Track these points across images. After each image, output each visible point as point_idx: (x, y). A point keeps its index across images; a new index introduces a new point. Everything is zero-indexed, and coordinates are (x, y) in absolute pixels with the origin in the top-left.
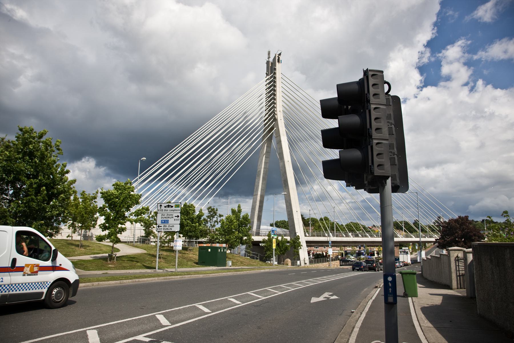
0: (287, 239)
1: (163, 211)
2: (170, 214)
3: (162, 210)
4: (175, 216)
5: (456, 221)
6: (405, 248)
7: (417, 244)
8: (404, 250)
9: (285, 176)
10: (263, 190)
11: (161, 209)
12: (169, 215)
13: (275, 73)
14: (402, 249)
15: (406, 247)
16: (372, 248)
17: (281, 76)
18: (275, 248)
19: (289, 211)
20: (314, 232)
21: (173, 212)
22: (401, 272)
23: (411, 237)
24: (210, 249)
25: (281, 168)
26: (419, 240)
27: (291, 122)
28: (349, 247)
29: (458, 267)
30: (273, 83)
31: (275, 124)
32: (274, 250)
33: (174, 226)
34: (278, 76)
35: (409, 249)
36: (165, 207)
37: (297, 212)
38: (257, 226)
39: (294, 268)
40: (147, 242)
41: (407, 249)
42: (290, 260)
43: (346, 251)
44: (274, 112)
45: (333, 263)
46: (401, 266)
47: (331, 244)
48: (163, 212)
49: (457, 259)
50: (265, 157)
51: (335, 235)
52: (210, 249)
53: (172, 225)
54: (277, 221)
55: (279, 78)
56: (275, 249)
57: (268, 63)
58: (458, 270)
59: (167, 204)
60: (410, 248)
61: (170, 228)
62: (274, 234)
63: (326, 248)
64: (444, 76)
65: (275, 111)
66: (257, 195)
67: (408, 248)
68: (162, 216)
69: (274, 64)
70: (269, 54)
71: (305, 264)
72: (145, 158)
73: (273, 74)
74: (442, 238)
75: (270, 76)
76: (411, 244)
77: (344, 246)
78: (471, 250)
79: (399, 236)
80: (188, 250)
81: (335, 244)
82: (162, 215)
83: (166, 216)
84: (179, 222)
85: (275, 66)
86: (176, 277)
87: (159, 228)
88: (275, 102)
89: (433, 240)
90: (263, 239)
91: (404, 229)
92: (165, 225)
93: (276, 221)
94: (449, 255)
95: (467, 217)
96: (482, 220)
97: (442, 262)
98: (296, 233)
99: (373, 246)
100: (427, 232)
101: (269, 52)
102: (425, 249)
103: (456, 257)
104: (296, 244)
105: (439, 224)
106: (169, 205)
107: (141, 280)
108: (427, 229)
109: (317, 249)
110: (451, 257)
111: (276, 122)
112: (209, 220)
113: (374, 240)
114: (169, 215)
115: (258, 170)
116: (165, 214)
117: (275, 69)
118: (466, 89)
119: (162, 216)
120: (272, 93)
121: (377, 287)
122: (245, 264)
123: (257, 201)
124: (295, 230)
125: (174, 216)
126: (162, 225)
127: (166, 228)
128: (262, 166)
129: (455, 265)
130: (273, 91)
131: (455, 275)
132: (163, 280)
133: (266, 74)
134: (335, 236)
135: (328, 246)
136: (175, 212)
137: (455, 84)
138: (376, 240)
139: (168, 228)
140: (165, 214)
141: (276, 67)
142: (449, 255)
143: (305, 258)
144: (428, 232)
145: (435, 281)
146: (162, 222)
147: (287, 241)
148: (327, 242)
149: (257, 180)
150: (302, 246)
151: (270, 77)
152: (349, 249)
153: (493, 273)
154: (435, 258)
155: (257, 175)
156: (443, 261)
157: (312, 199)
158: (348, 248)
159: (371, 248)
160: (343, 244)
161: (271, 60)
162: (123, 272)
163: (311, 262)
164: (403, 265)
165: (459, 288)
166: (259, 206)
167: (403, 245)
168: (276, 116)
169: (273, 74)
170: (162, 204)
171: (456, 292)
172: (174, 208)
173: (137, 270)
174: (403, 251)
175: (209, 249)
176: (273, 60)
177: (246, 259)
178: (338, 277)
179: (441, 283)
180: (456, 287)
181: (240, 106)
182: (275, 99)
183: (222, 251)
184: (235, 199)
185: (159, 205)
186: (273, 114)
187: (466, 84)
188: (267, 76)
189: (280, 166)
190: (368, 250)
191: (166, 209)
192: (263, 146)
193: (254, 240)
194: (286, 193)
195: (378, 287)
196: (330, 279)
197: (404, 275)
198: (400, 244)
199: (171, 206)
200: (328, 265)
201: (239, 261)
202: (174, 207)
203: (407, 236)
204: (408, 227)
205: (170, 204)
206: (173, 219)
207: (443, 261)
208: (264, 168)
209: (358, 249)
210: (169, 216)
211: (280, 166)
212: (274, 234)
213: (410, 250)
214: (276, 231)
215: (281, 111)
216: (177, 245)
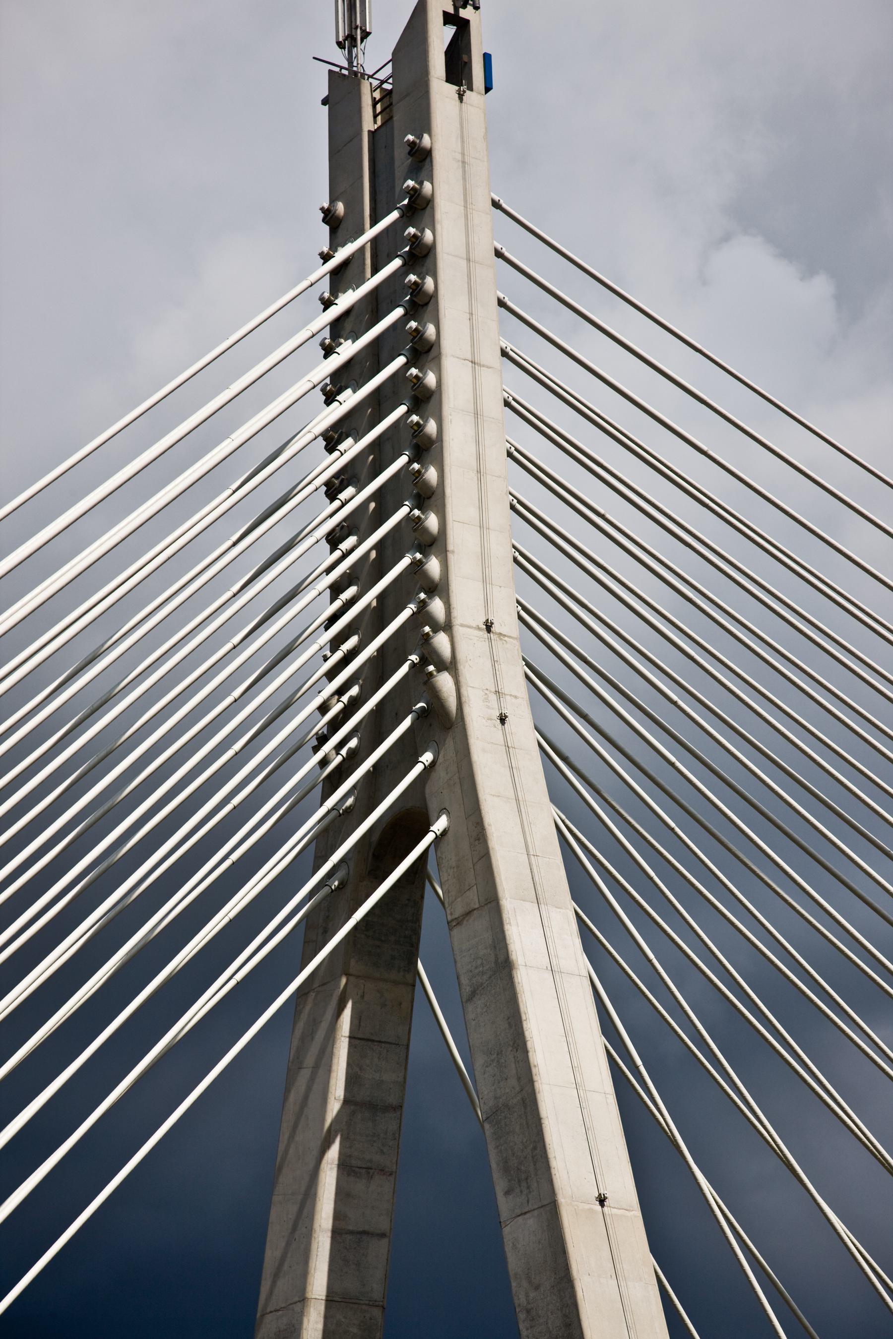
24: (422, 593)
25: (520, 1294)
31: (440, 772)
50: (344, 1166)
65: (436, 628)
75: (371, 233)
85: (424, 124)
88: (432, 522)
111: (450, 744)
130: (402, 409)
133: (329, 216)
141: (426, 140)
151: (375, 241)
168: (444, 682)
169: (395, 215)
188: (336, 242)
189: (514, 1263)
208: (330, 1300)
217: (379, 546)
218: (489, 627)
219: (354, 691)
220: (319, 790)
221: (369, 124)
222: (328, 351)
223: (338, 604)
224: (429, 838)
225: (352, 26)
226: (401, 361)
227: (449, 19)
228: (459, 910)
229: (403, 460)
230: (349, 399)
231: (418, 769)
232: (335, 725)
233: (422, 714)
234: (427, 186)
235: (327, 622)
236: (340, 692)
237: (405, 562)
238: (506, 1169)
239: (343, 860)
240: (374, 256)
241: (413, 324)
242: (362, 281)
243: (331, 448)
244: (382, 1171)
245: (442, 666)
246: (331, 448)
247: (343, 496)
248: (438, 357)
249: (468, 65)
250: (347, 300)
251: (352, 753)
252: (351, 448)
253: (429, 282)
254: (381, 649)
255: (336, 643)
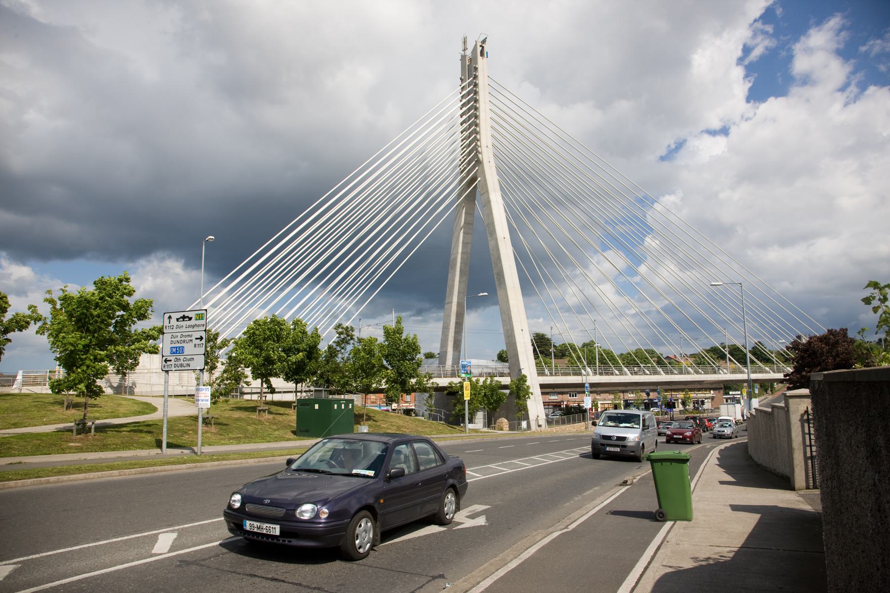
3: (172, 327)
4: (196, 339)
5: (823, 339)
6: (734, 393)
7: (758, 385)
8: (732, 396)
11: (170, 325)
12: (186, 336)
13: (476, 77)
14: (729, 394)
17: (487, 81)
20: (569, 366)
21: (193, 330)
23: (767, 372)
24: (317, 405)
25: (491, 252)
26: (747, 379)
32: (467, 403)
35: (741, 394)
36: (178, 320)
37: (522, 330)
38: (453, 359)
39: (516, 435)
41: (738, 394)
42: (506, 421)
43: (626, 401)
44: (475, 148)
47: (589, 388)
49: (805, 417)
50: (464, 233)
52: (317, 405)
53: (190, 357)
54: (503, 350)
55: (484, 85)
56: (468, 400)
57: (463, 58)
58: (808, 443)
59: (181, 314)
60: (743, 392)
61: (188, 362)
66: (452, 302)
67: (739, 393)
68: (172, 339)
69: (473, 60)
70: (464, 42)
71: (540, 426)
72: (213, 238)
73: (472, 78)
74: (797, 370)
75: (468, 81)
76: (745, 384)
77: (623, 392)
78: (805, 391)
80: (293, 407)
81: (596, 388)
82: (173, 337)
83: (179, 339)
85: (476, 63)
86: (178, 466)
88: (478, 129)
89: (780, 376)
90: (450, 384)
91: (729, 358)
92: (177, 357)
93: (501, 350)
95: (844, 331)
96: (879, 340)
97: (776, 423)
98: (520, 370)
99: (675, 390)
100: (774, 363)
101: (465, 39)
102: (772, 393)
103: (803, 412)
104: (519, 391)
105: (795, 346)
107: (65, 478)
109: (575, 398)
110: (791, 413)
111: (481, 166)
112: (338, 349)
114: (186, 336)
115: (452, 257)
117: (476, 69)
119: (173, 339)
120: (472, 113)
123: (452, 313)
125: (193, 338)
126: (173, 358)
129: (801, 433)
130: (473, 111)
131: (802, 455)
132: (135, 474)
133: (461, 79)
134: (598, 373)
135: (584, 392)
139: (183, 362)
140: (177, 334)
142: (786, 409)
143: (538, 416)
144: (775, 362)
145: (764, 464)
146: (172, 353)
148: (582, 385)
149: (450, 276)
151: (469, 83)
152: (631, 396)
157: (568, 309)
158: (629, 396)
159: (671, 395)
160: (621, 388)
161: (469, 53)
163: (549, 422)
165: (811, 487)
166: (457, 323)
168: (480, 156)
169: (472, 78)
170: (172, 315)
172: (193, 322)
173: (120, 452)
174: (730, 398)
175: (316, 405)
177: (410, 422)
179: (774, 470)
180: (804, 484)
181: (438, 153)
183: (343, 408)
185: (167, 316)
186: (475, 152)
188: (462, 83)
189: (490, 247)
190: (665, 397)
191: (179, 323)
193: (440, 386)
197: (655, 464)
198: (724, 386)
199: (188, 317)
200: (584, 428)
202: (193, 319)
203: (734, 372)
204: (741, 354)
205: (186, 314)
206: (191, 345)
207: (778, 422)
209: (644, 395)
213: (744, 395)
215: (490, 146)
216: (200, 398)
217: (469, 133)
219: (465, 157)
220: (459, 174)
221: (468, 63)
223: (462, 143)
225: (465, 47)
228: (482, 193)
231: (475, 170)
232: (462, 163)
233: (476, 161)
235: (624, 416)
236: (463, 157)
237: (474, 136)
238: (489, 233)
239: (464, 185)
240: (469, 85)
241: (475, 89)
244: (470, 233)
249: (484, 53)
250: (464, 93)
251: (465, 167)
254: (470, 150)
255: (462, 149)
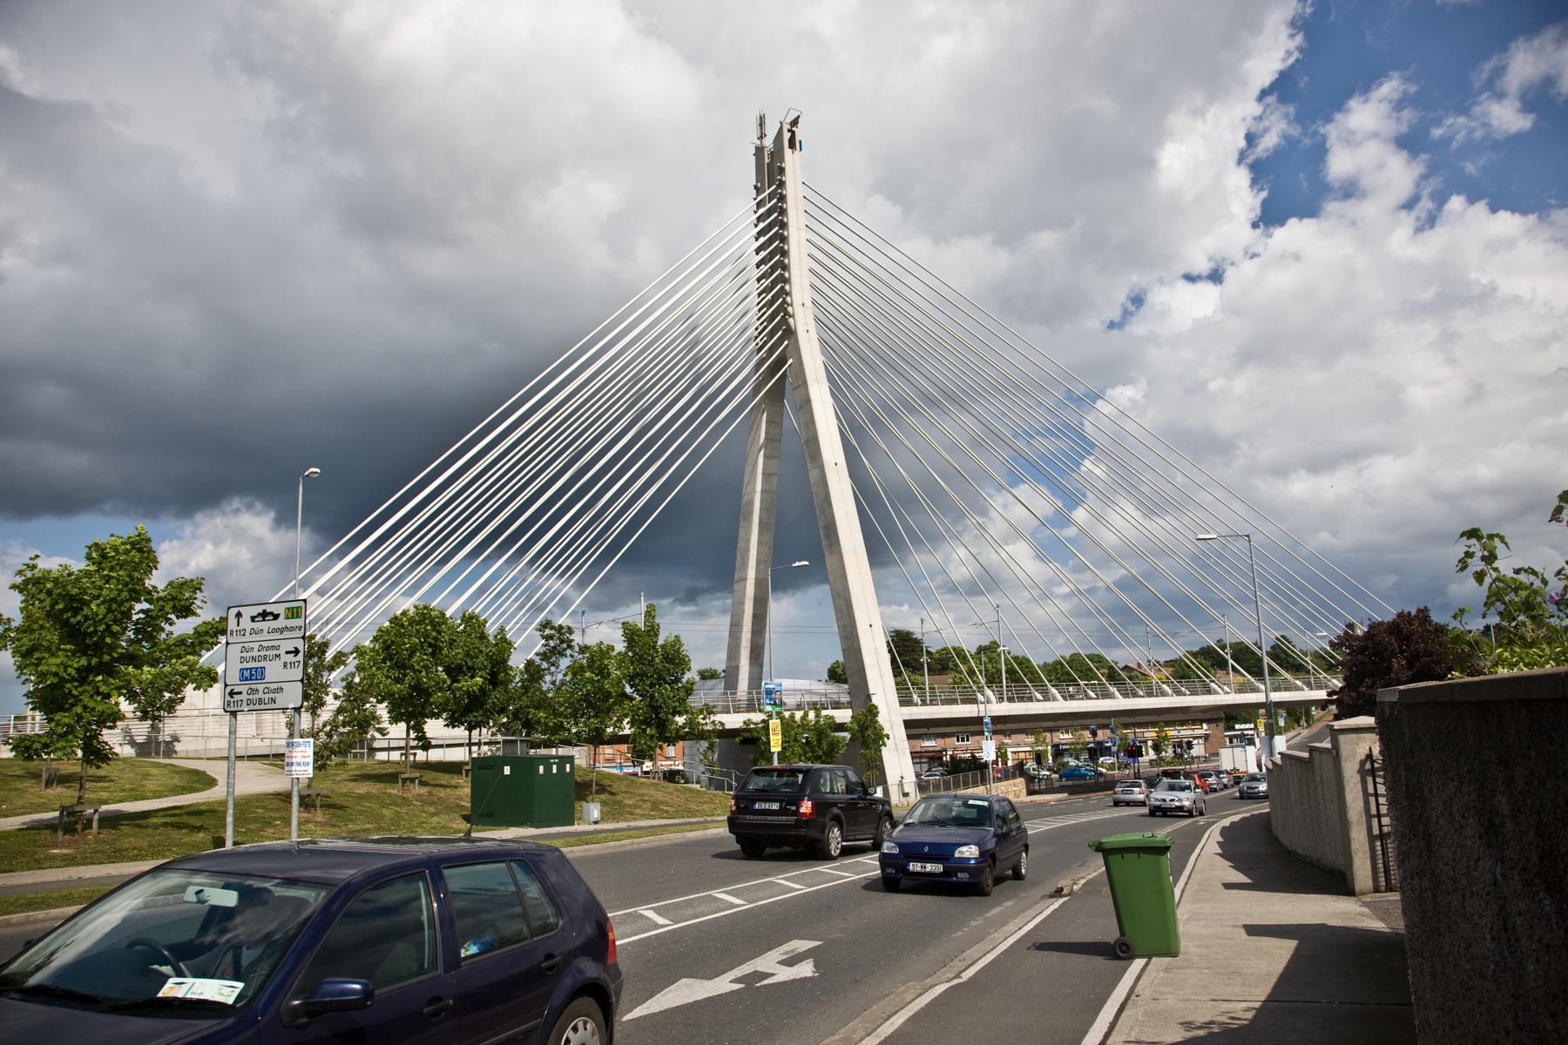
0: (832, 717)
1: (247, 633)
2: (270, 644)
3: (242, 633)
4: (287, 652)
6: (1243, 726)
7: (1283, 712)
8: (1239, 732)
9: (826, 512)
10: (765, 562)
11: (238, 628)
12: (268, 648)
13: (782, 184)
15: (1246, 723)
16: (1138, 730)
17: (803, 190)
18: (779, 749)
19: (845, 627)
21: (282, 637)
22: (1100, 843)
25: (814, 489)
27: (839, 333)
28: (1067, 733)
29: (1372, 799)
30: (776, 214)
31: (790, 348)
32: (776, 757)
33: (282, 689)
34: (793, 190)
35: (1256, 728)
36: (253, 619)
37: (871, 626)
38: (749, 679)
40: (358, 751)
41: (1251, 729)
43: (1056, 746)
44: (783, 308)
45: (1003, 788)
46: (1226, 787)
47: (990, 726)
48: (248, 638)
49: (1368, 766)
50: (765, 456)
51: (1005, 697)
56: (779, 753)
57: (759, 151)
58: (1374, 812)
61: (271, 695)
62: (772, 702)
63: (971, 742)
64: (1337, 185)
65: (788, 305)
67: (1252, 726)
68: (243, 655)
69: (777, 154)
70: (761, 124)
71: (906, 795)
72: (319, 471)
73: (774, 186)
75: (768, 192)
76: (1262, 711)
77: (1051, 730)
78: (1367, 721)
79: (1214, 690)
80: (464, 772)
81: (1004, 725)
82: (244, 650)
83: (256, 653)
84: (298, 673)
85: (782, 160)
87: (232, 700)
88: (787, 275)
91: (1233, 666)
92: (253, 687)
93: (834, 661)
94: (1334, 751)
96: (1485, 627)
97: (1318, 778)
98: (869, 697)
99: (1141, 725)
100: (1309, 670)
101: (761, 118)
103: (1363, 757)
105: (1345, 641)
106: (264, 611)
108: (1308, 664)
109: (966, 743)
110: (1343, 759)
112: (545, 665)
113: (1133, 705)
114: (268, 648)
115: (745, 499)
116: (251, 645)
117: (782, 171)
118: (1407, 222)
119: (244, 654)
121: (1062, 889)
122: (666, 812)
124: (867, 686)
125: (282, 651)
126: (244, 689)
127: (257, 696)
128: (755, 485)
129: (1361, 794)
130: (778, 242)
131: (1365, 832)
133: (756, 187)
134: (1005, 699)
135: (981, 733)
136: (286, 634)
137: (1368, 210)
138: (1140, 704)
139: (262, 696)
140: (251, 645)
141: (783, 165)
142: (1334, 751)
143: (902, 778)
144: (1312, 671)
145: (1300, 851)
146: (243, 678)
147: (835, 723)
148: (978, 721)
149: (742, 533)
150: (888, 738)
151: (769, 194)
152: (1064, 737)
153: (1505, 929)
154: (1294, 762)
155: (741, 517)
156: (1321, 776)
158: (1062, 737)
160: (1046, 724)
161: (769, 142)
162: (50, 879)
164: (1232, 783)
165: (1383, 889)
166: (755, 616)
167: (1239, 717)
168: (791, 321)
169: (774, 186)
171: (1366, 910)
172: (281, 623)
174: (1236, 736)
176: (774, 142)
178: (1045, 825)
180: (1369, 884)
182: (785, 267)
183: (555, 771)
184: (716, 603)
186: (782, 314)
187: (1409, 205)
188: (758, 195)
189: (812, 481)
191: (256, 625)
192: (758, 421)
193: (727, 727)
194: (807, 563)
195: (1065, 891)
196: (1052, 825)
198: (1226, 715)
199: (271, 613)
201: (646, 801)
205: (269, 609)
206: (279, 664)
207: (1321, 776)
208: (762, 492)
209: (1087, 735)
210: (267, 653)
211: (809, 481)
212: (772, 702)
213: (1260, 730)
214: (780, 691)
215: (808, 303)
216: (294, 760)
217: (771, 282)
218: (803, 305)
219: (765, 324)
221: (767, 161)
222: (756, 226)
223: (760, 299)
224: (787, 365)
225: (762, 134)
226: (777, 228)
227: (789, 131)
228: (796, 385)
229: (778, 257)
230: (762, 240)
231: (784, 346)
232: (760, 334)
234: (784, 178)
236: (761, 324)
237: (779, 286)
238: (810, 456)
241: (780, 204)
242: (765, 205)
243: (757, 254)
245: (790, 316)
246: (757, 254)
247: (761, 268)
248: (787, 227)
250: (761, 211)
252: (763, 254)
253: (785, 205)
254: (773, 312)
255: (760, 310)
